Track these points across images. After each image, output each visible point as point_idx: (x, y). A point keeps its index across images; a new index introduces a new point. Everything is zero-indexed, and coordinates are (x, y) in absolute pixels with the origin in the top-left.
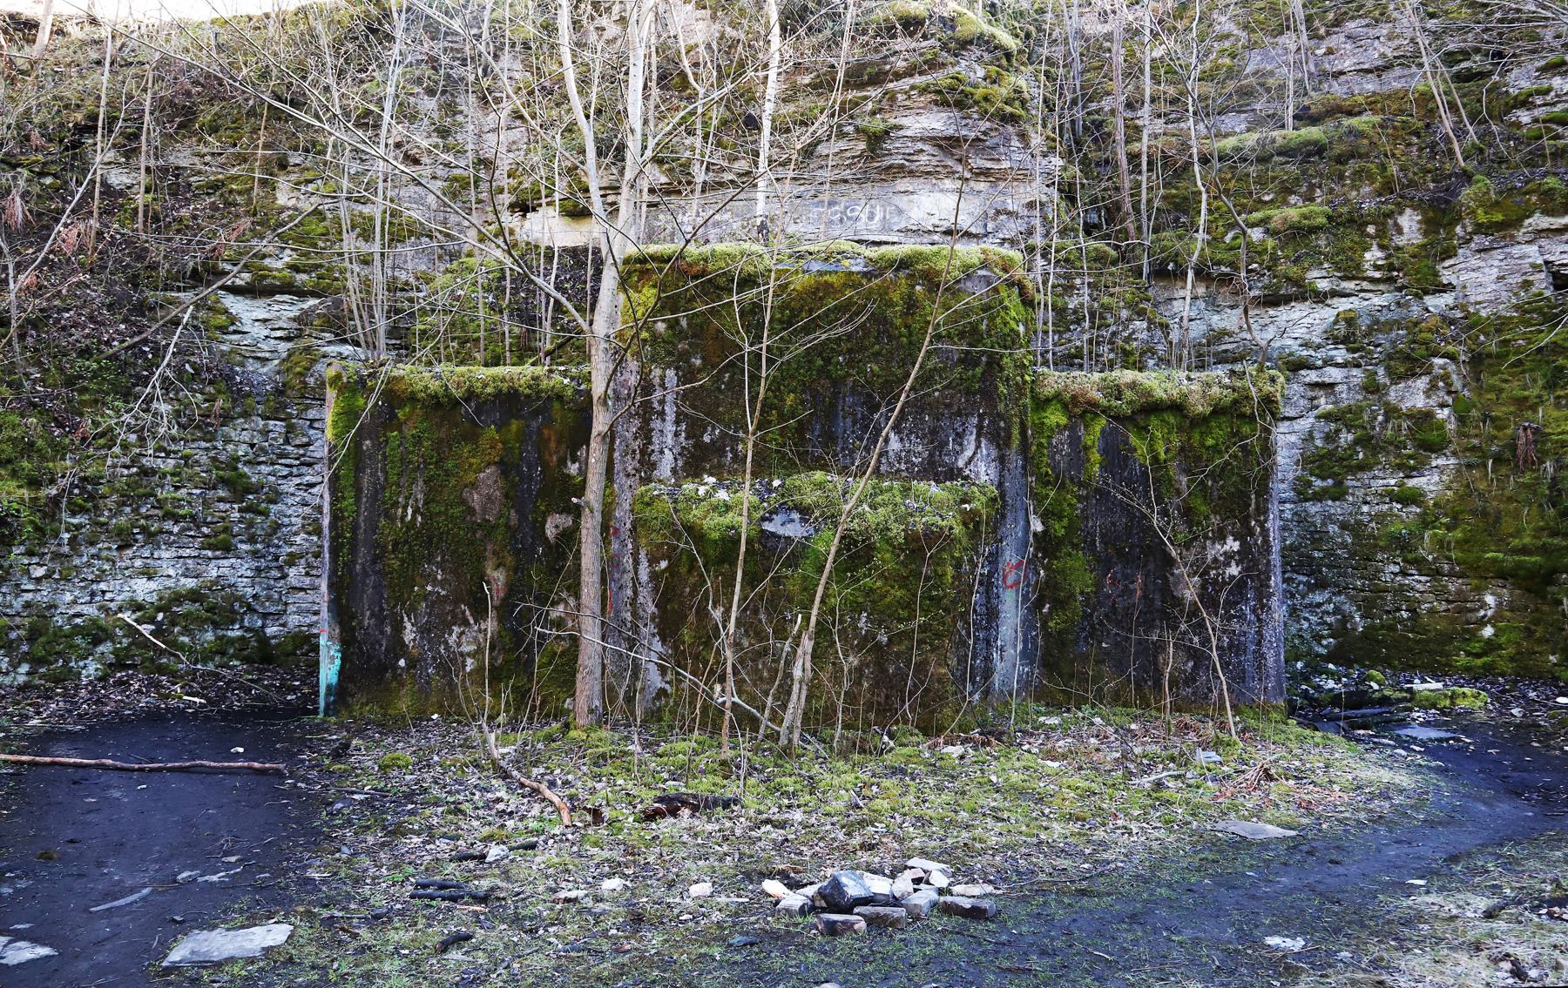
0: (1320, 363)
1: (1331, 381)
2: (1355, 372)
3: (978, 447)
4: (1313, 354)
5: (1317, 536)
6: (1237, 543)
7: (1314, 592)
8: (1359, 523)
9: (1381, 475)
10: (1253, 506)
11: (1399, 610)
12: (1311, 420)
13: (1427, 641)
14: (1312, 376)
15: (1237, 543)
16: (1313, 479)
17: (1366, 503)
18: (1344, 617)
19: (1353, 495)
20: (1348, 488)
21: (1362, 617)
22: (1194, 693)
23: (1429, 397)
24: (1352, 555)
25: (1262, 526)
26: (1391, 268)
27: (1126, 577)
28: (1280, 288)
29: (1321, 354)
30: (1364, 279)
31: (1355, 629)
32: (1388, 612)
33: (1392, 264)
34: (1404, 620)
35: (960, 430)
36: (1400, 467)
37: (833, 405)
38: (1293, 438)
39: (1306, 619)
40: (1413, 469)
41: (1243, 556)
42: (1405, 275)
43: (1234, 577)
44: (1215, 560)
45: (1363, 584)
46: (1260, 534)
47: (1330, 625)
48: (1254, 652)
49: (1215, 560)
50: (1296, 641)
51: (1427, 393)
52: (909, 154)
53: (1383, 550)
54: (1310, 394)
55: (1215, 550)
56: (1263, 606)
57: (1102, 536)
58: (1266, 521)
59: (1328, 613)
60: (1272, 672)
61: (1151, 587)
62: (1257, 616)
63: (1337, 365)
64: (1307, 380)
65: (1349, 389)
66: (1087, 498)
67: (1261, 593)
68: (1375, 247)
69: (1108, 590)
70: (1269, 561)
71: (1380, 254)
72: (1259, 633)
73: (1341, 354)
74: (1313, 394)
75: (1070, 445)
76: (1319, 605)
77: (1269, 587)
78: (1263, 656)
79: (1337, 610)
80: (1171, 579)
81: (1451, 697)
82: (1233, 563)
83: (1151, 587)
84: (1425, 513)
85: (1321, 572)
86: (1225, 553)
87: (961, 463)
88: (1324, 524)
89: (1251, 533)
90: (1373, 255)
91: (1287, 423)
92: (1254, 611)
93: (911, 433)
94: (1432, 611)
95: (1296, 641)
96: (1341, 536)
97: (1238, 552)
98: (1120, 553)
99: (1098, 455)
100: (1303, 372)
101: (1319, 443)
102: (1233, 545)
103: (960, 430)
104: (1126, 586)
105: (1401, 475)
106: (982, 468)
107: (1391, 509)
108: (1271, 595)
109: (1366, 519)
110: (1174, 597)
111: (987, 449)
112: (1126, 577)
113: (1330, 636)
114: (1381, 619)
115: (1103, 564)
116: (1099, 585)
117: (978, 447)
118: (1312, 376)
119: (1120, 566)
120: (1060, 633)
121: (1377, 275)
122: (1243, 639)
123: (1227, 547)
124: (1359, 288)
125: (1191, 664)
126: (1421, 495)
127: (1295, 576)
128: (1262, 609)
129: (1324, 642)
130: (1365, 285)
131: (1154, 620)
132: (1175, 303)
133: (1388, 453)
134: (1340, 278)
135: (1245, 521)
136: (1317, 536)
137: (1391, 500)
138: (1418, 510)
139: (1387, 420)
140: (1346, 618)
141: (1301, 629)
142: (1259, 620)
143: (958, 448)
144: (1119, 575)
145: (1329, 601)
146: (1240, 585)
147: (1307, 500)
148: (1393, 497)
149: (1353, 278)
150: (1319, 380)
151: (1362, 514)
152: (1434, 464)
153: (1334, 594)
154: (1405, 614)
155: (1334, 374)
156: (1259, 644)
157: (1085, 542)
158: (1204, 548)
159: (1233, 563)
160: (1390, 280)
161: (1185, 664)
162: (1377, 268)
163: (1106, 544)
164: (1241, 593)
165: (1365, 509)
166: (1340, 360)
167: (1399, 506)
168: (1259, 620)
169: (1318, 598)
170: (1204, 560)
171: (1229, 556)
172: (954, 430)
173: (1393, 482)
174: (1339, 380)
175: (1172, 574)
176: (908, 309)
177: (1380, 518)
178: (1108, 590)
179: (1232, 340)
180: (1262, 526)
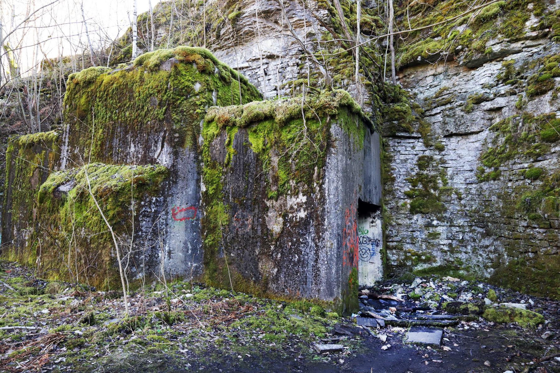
0: (492, 96)
1: (498, 106)
2: (513, 97)
3: (163, 147)
4: (488, 91)
5: (487, 203)
6: (305, 197)
7: (484, 238)
8: (507, 194)
9: (519, 161)
10: (316, 174)
11: (526, 252)
12: (487, 132)
13: (543, 275)
14: (488, 105)
15: (305, 197)
16: (485, 168)
17: (510, 181)
18: (499, 255)
19: (503, 176)
20: (501, 171)
21: (508, 256)
22: (277, 288)
23: (552, 105)
24: (503, 214)
25: (320, 186)
26: (542, 27)
27: (243, 217)
28: (472, 56)
29: (494, 90)
30: (527, 39)
31: (504, 263)
32: (521, 253)
33: (543, 24)
34: (531, 259)
35: (156, 140)
36: (529, 155)
37: (113, 133)
38: (477, 145)
39: (481, 255)
40: (539, 155)
41: (309, 204)
42: (553, 29)
43: (302, 218)
44: (292, 208)
45: (509, 233)
46: (320, 191)
47: (492, 260)
48: (313, 266)
49: (292, 208)
50: (477, 269)
51: (551, 103)
52: (250, 25)
53: (518, 210)
54: (488, 116)
55: (292, 201)
56: (319, 238)
57: (233, 194)
58: (323, 183)
59: (491, 252)
60: (324, 280)
61: (256, 223)
62: (316, 244)
63: (502, 95)
64: (485, 108)
65: (509, 109)
66: (226, 173)
67: (318, 229)
68: (532, 17)
69: (234, 224)
70: (324, 209)
71: (536, 20)
72: (317, 254)
73: (503, 89)
74: (490, 116)
75: (220, 144)
76: (487, 247)
77: (323, 225)
78: (318, 270)
79: (496, 251)
80: (267, 218)
81: (510, 315)
82: (302, 210)
83: (256, 223)
84: (545, 185)
85: (488, 226)
86: (298, 203)
87: (156, 156)
88: (490, 196)
89: (313, 190)
90: (533, 22)
91: (475, 136)
92: (313, 240)
93: (139, 143)
94: (547, 254)
95: (477, 269)
96: (497, 203)
97: (306, 203)
98: (241, 204)
99: (232, 149)
100: (483, 104)
101: (490, 146)
102: (302, 199)
103: (156, 140)
104: (243, 222)
105: (532, 160)
106: (164, 158)
107: (524, 183)
108: (324, 231)
109: (510, 191)
110: (268, 229)
111: (167, 148)
112: (243, 217)
113: (492, 267)
114: (518, 257)
115: (234, 209)
116: (230, 221)
117: (163, 147)
118: (488, 105)
119: (241, 210)
120: (211, 246)
121: (534, 34)
122: (306, 257)
123: (299, 200)
124: (524, 45)
125: (276, 270)
126: (543, 173)
127: (477, 228)
128: (319, 239)
129: (489, 270)
130: (528, 43)
131: (257, 242)
132: (427, 79)
133: (523, 146)
134: (508, 42)
135: (310, 182)
136: (487, 203)
137: (525, 178)
138: (541, 183)
139: (523, 125)
140: (500, 256)
141: (478, 261)
142: (317, 246)
143: (155, 148)
144: (240, 216)
145: (492, 244)
146: (305, 223)
147: (481, 181)
148: (524, 175)
149: (517, 40)
150: (492, 107)
151: (508, 188)
152: (553, 150)
153: (495, 240)
154: (531, 255)
155: (500, 102)
156: (316, 261)
157: (225, 197)
158: (286, 200)
159: (302, 210)
160: (545, 36)
161: (273, 269)
162: (533, 29)
163: (234, 198)
164: (306, 229)
165: (510, 184)
166: (503, 92)
167: (529, 181)
168: (317, 246)
169: (486, 242)
170: (285, 205)
171: (300, 205)
172: (154, 139)
173: (526, 165)
174: (503, 105)
175: (267, 216)
176: (141, 83)
177: (517, 190)
178: (234, 224)
179: (448, 92)
180: (320, 186)
